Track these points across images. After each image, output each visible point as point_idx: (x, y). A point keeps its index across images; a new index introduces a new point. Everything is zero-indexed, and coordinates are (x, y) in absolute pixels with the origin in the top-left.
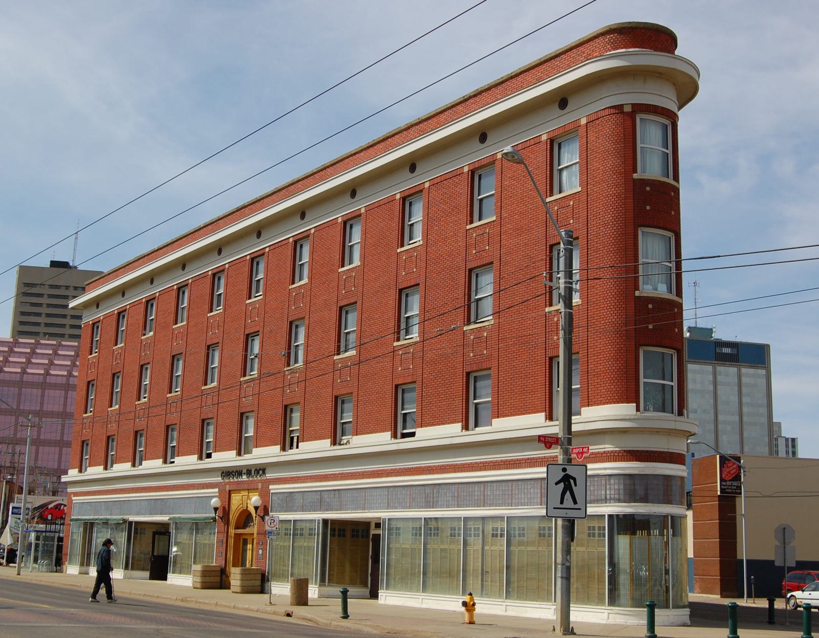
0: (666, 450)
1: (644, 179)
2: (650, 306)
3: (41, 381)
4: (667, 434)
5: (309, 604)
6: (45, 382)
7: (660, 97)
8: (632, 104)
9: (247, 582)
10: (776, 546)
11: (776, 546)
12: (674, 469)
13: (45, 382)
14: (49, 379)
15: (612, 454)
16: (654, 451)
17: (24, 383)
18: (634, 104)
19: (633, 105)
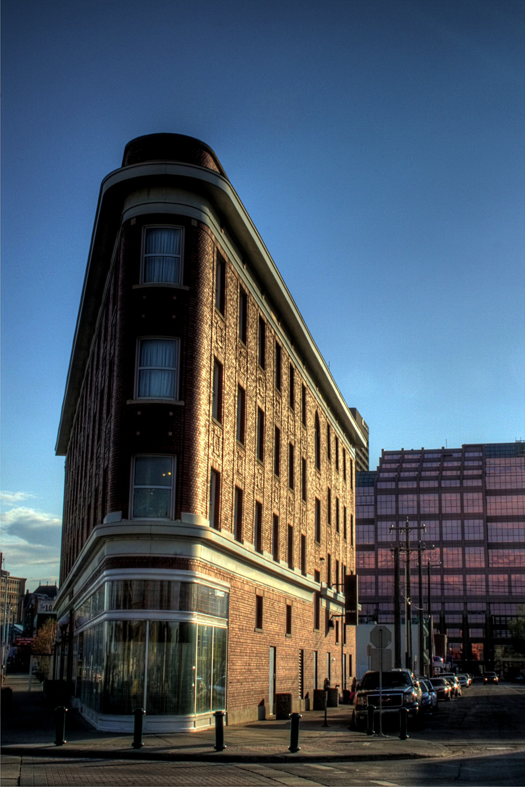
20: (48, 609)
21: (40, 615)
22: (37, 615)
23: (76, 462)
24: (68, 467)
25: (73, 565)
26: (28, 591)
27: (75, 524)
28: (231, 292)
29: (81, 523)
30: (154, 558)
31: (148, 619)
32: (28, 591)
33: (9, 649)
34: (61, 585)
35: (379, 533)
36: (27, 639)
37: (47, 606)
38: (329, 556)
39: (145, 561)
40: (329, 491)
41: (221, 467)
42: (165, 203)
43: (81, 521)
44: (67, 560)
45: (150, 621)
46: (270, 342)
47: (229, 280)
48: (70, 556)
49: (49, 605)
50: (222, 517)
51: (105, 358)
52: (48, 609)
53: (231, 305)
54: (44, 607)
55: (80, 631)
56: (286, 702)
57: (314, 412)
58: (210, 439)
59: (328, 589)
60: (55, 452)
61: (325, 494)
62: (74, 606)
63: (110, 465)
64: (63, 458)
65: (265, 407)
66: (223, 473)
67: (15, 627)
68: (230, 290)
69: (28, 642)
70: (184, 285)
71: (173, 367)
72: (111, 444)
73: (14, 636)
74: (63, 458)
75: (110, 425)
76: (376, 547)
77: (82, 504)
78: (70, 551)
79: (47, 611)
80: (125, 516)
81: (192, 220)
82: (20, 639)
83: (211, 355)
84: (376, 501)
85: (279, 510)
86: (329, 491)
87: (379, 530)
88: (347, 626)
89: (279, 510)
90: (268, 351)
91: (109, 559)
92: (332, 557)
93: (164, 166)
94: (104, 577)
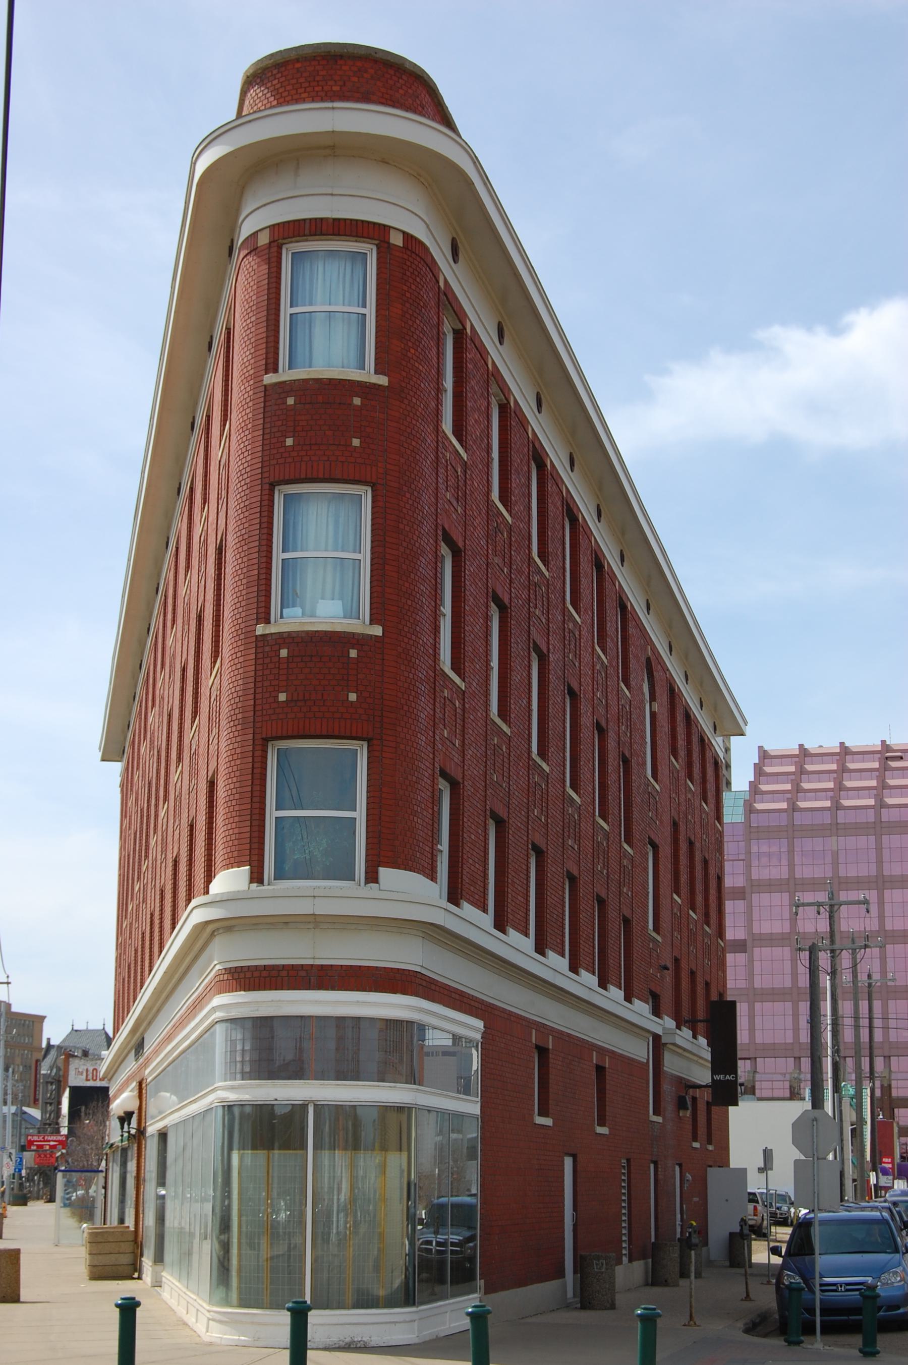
0: (310, 962)
1: (285, 382)
2: (353, 653)
3: (872, 819)
4: (311, 926)
5: (22, 1300)
6: (879, 821)
7: (330, 197)
8: (269, 227)
9: (100, 1257)
10: (797, 1162)
11: (797, 1162)
12: (327, 1003)
13: (879, 821)
14: (885, 815)
15: (256, 974)
16: (278, 966)
17: (752, 830)
18: (274, 226)
19: (272, 228)
20: (90, 1077)
21: (75, 1091)
22: (68, 1090)
23: (144, 771)
24: (126, 786)
25: (142, 987)
26: (49, 1039)
27: (144, 901)
28: (475, 392)
29: (158, 897)
30: (322, 967)
31: (310, 1101)
32: (49, 1039)
33: (13, 1157)
34: (116, 1029)
35: (755, 916)
36: (49, 1138)
37: (87, 1070)
38: (677, 961)
39: (303, 974)
40: (675, 825)
41: (460, 770)
42: (332, 195)
43: (158, 893)
44: (129, 977)
45: (315, 1105)
46: (555, 505)
47: (470, 366)
48: (136, 966)
49: (91, 1069)
50: (464, 877)
51: (206, 540)
52: (90, 1077)
53: (476, 421)
54: (81, 1074)
55: (160, 1125)
56: (602, 1273)
57: (643, 660)
58: (438, 710)
59: (678, 1031)
60: (99, 755)
61: (667, 830)
62: (147, 1071)
63: (222, 769)
64: (117, 768)
65: (548, 643)
66: (466, 783)
67: (25, 1113)
68: (472, 388)
69: (52, 1143)
70: (377, 372)
71: (354, 552)
72: (224, 723)
73: (23, 1130)
74: (117, 768)
75: (221, 681)
76: (749, 944)
77: (159, 857)
78: (136, 957)
79: (87, 1080)
80: (257, 877)
81: (392, 231)
82: (36, 1138)
83: (436, 526)
84: (749, 852)
85: (578, 864)
86: (675, 825)
87: (756, 911)
88: (714, 1109)
89: (578, 864)
90: (550, 525)
91: (229, 971)
92: (684, 964)
93: (329, 113)
94: (214, 1009)
